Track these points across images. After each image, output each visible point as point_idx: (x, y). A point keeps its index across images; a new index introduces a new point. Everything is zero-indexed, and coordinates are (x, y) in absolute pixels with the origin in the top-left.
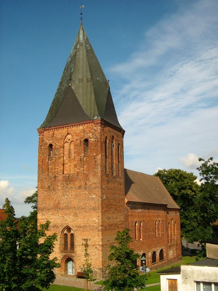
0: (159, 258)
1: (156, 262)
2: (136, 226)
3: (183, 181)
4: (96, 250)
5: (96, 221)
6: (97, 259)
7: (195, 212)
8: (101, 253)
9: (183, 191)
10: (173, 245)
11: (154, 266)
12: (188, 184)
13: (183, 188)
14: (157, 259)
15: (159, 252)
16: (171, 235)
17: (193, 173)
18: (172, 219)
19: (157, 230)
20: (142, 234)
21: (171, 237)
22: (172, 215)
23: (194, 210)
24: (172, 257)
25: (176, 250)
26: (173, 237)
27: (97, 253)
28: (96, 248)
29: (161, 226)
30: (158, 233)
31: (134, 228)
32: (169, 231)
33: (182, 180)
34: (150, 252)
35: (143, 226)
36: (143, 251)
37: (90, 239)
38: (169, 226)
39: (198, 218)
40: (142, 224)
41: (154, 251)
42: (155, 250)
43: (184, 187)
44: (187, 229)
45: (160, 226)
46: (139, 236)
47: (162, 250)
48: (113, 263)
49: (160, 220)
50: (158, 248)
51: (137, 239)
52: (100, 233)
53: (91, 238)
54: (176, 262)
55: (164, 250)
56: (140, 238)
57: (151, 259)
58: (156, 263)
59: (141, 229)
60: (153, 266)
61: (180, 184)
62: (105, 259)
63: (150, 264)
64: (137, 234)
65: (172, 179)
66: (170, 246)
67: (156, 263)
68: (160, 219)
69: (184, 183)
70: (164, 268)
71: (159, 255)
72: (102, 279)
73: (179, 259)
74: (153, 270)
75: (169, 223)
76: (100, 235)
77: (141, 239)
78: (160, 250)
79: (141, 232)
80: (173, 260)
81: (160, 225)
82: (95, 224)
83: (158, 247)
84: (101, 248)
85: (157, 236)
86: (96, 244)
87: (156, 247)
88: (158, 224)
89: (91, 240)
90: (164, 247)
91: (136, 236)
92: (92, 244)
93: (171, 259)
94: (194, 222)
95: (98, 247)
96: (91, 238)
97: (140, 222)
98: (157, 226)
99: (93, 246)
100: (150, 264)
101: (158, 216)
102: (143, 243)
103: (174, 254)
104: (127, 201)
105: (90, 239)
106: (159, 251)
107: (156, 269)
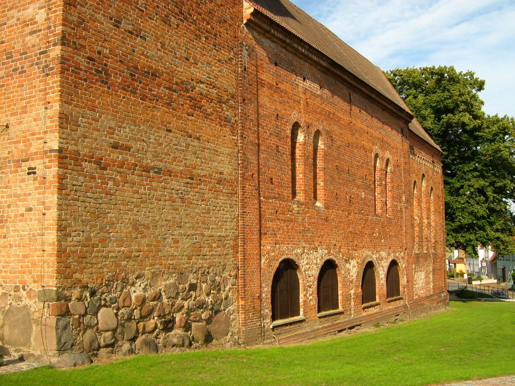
0: (385, 288)
1: (375, 300)
2: (297, 145)
3: (449, 91)
4: (30, 185)
5: (38, 18)
6: (33, 238)
7: (478, 177)
8: (52, 198)
9: (445, 118)
10: (426, 257)
11: (369, 313)
12: (463, 98)
13: (447, 110)
14: (377, 290)
15: (386, 269)
16: (421, 223)
17: (474, 74)
18: (423, 175)
19: (378, 190)
20: (321, 183)
21: (421, 230)
22: (424, 163)
23: (477, 173)
24: (422, 293)
25: (433, 274)
26: (426, 231)
27: (32, 203)
28: (32, 171)
29: (392, 182)
30: (384, 199)
31: (288, 148)
32: (416, 211)
33: (445, 87)
34: (353, 262)
35: (326, 154)
36: (326, 251)
37: (7, 127)
38: (415, 192)
39: (487, 193)
40: (321, 145)
41: (367, 261)
42: (371, 257)
43: (452, 106)
44: (459, 221)
45: (388, 180)
46: (312, 187)
47: (394, 264)
48: (155, 275)
49: (388, 159)
50: (383, 254)
51: (300, 197)
52: (55, 81)
53: (12, 119)
54: (435, 308)
55: (402, 265)
56: (315, 198)
57: (357, 287)
58: (373, 303)
59: (320, 164)
60: (364, 314)
61: (438, 99)
62: (88, 239)
63: (353, 303)
64: (299, 176)
65: (416, 89)
66: (417, 256)
67: (377, 304)
68: (388, 155)
69: (451, 97)
70: (401, 323)
71: (384, 279)
72: (54, 360)
73: (440, 302)
74: (367, 330)
75: (415, 182)
76: (54, 96)
77: (318, 204)
78: (390, 260)
79: (320, 174)
80: (426, 303)
81: (389, 176)
82: (32, 40)
83: (383, 250)
84: (53, 171)
85: (379, 211)
86: (33, 150)
87: (375, 248)
88: (381, 170)
89: (12, 129)
90: (402, 254)
91: (297, 184)
92: (15, 152)
93: (421, 299)
94: (478, 204)
95: (36, 163)
96: (12, 119)
97: (313, 130)
98: (378, 174)
99: (18, 163)
100: (353, 303)
101: (384, 145)
102: (327, 220)
103: (428, 283)
104: (252, 10)
105: (7, 127)
106: (386, 264)
107: (377, 325)
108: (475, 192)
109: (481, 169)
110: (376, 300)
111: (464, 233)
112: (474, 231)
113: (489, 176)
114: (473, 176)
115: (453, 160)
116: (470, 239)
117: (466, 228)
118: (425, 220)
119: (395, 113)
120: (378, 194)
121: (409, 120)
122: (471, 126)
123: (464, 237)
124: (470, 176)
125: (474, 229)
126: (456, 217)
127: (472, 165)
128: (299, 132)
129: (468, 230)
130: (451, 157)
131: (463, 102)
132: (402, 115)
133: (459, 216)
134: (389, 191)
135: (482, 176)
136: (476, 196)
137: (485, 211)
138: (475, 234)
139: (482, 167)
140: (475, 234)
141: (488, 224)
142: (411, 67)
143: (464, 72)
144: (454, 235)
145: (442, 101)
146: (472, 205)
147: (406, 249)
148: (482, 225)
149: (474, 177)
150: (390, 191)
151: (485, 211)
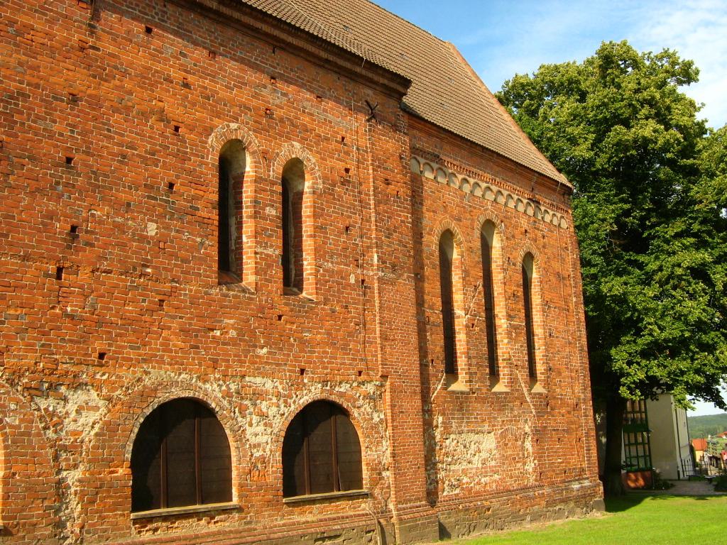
9: (618, 133)
23: (692, 240)
43: (627, 113)
44: (651, 335)
108: (685, 275)
109: (699, 230)
110: (231, 500)
111: (666, 357)
112: (691, 354)
113: (718, 243)
114: (684, 245)
115: (642, 219)
116: (681, 370)
117: (668, 347)
118: (503, 321)
119: (327, 61)
120: (248, 237)
121: (401, 89)
122: (661, 142)
123: (665, 367)
124: (677, 244)
125: (688, 350)
126: (646, 328)
127: (679, 225)
128: (495, 232)
129: (674, 354)
130: (637, 213)
131: (643, 102)
132: (358, 70)
133: (649, 324)
134: (308, 236)
135: (701, 244)
136: (690, 283)
137: (704, 310)
138: (693, 360)
139: (700, 227)
140: (693, 360)
141: (722, 338)
142: (559, 61)
143: (657, 51)
144: (644, 362)
145: (604, 104)
146: (680, 302)
147: (384, 377)
148: (711, 342)
149: (686, 248)
150: (311, 236)
151: (704, 310)
